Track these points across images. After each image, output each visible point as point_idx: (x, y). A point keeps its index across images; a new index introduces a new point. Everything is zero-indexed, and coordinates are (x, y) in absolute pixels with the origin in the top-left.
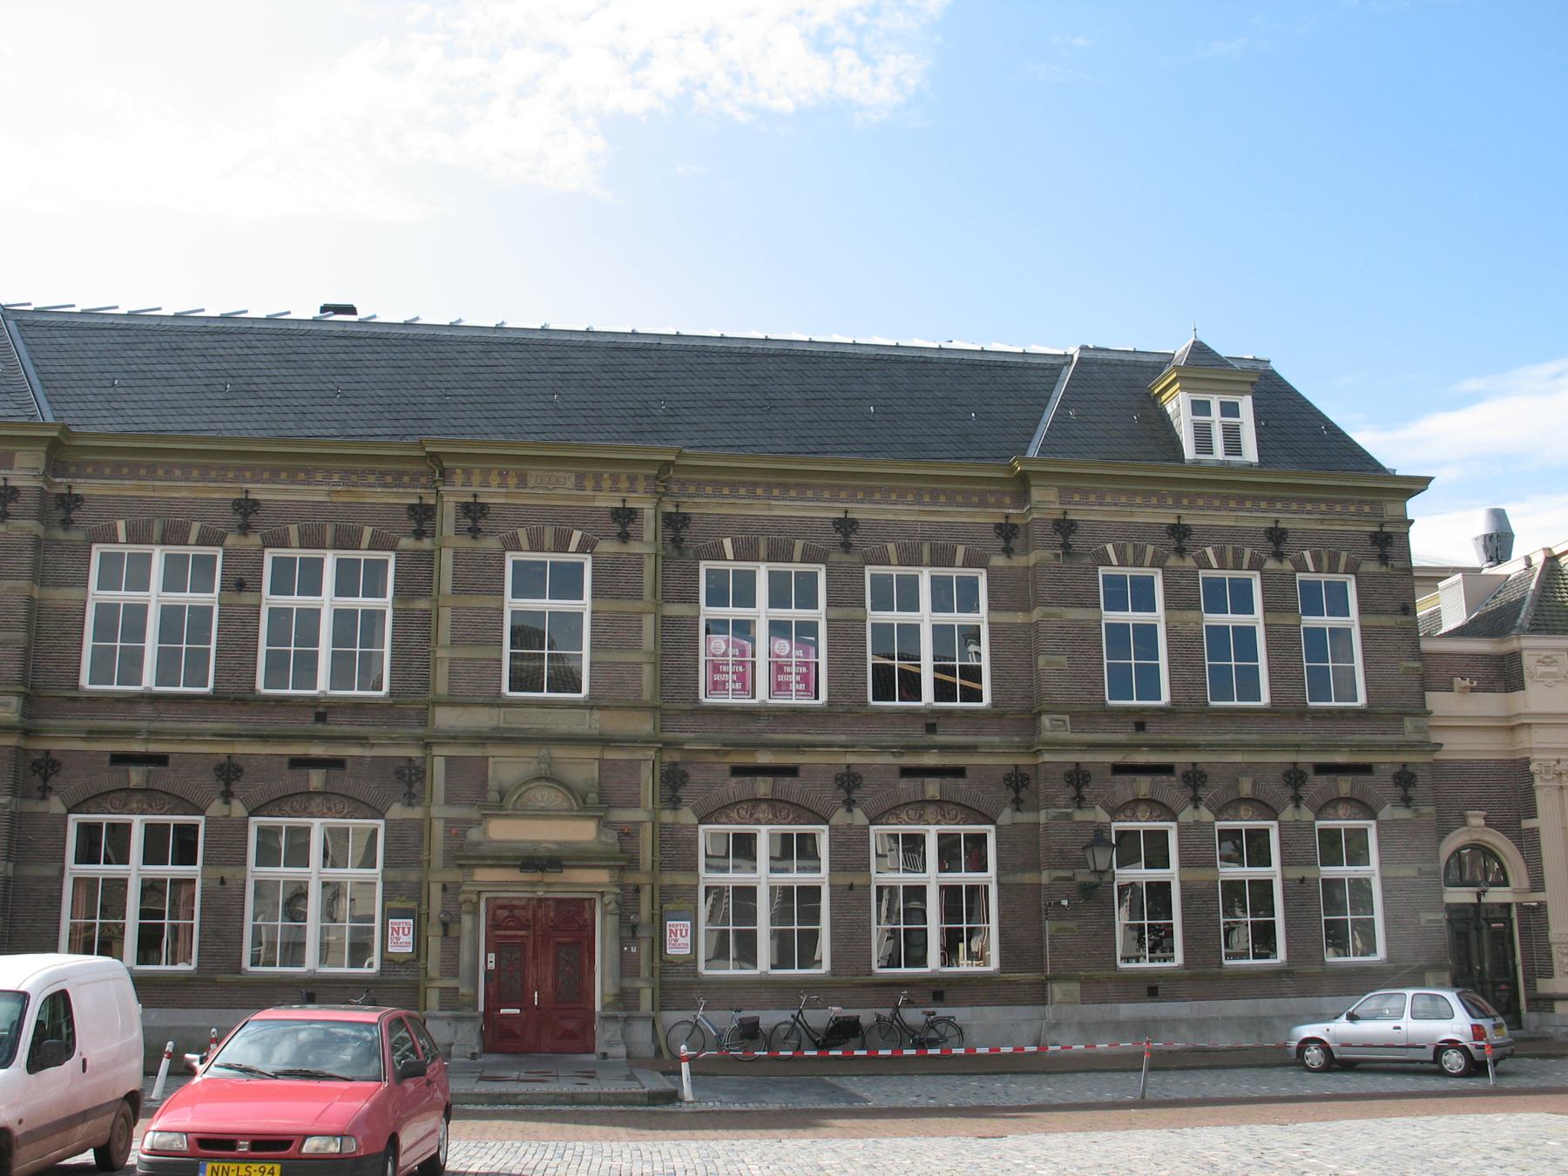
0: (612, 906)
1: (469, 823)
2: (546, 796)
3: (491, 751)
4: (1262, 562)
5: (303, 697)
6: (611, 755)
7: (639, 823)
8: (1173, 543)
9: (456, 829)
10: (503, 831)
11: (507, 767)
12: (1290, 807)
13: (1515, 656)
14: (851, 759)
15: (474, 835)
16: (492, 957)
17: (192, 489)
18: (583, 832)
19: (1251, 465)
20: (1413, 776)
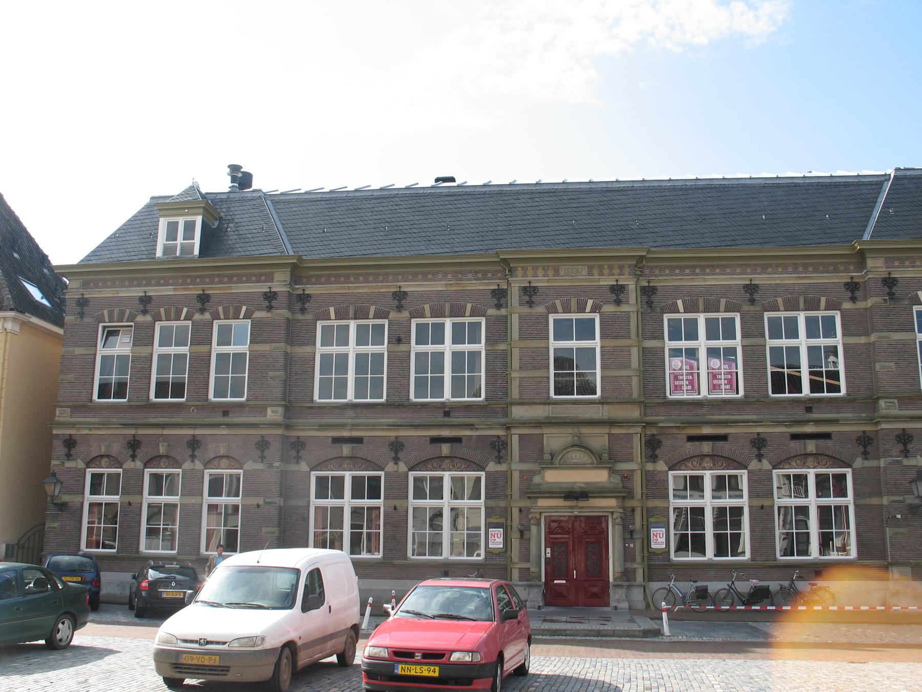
0: (619, 520)
1: (534, 473)
2: (578, 456)
3: (545, 431)
6: (615, 431)
7: (633, 471)
9: (526, 476)
10: (553, 477)
14: (73, 432)
15: (537, 479)
16: (549, 550)
18: (600, 477)
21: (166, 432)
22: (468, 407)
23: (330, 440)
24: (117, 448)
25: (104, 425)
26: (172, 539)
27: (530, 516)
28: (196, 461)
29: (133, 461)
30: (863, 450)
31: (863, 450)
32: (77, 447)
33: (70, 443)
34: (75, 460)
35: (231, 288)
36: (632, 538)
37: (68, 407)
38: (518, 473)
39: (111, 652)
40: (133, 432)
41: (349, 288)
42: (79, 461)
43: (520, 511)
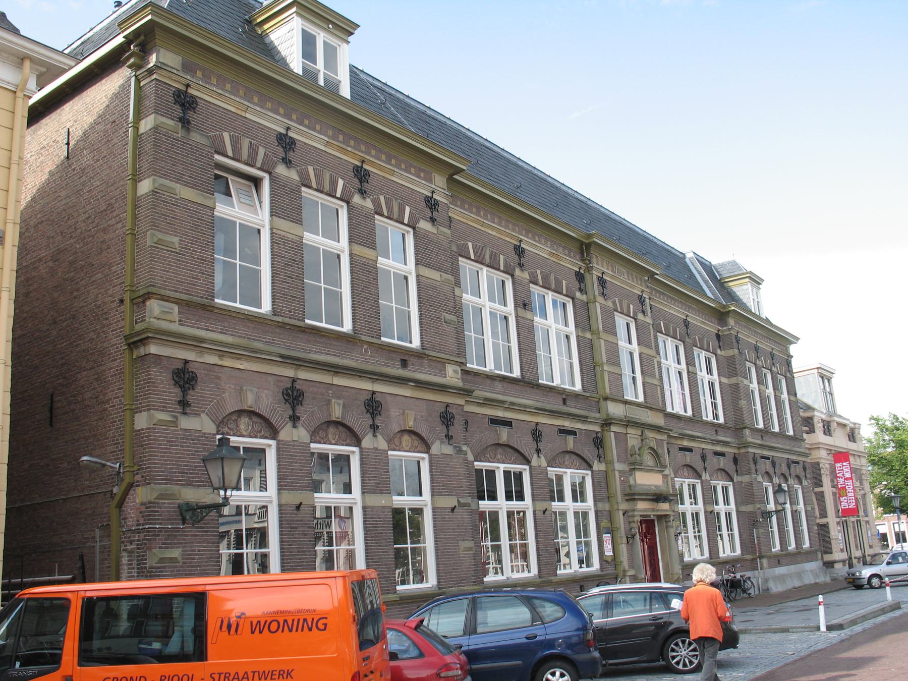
4: (274, 165)
5: (402, 346)
8: (280, 152)
12: (370, 435)
14: (190, 355)
17: (498, 231)
20: (379, 404)
21: (339, 381)
22: (504, 379)
23: (487, 420)
24: (265, 400)
25: (254, 355)
26: (525, 556)
28: (380, 437)
29: (295, 426)
30: (291, 413)
31: (291, 413)
32: (198, 388)
33: (185, 377)
34: (196, 414)
35: (393, 173)
37: (178, 302)
40: (290, 372)
41: (483, 224)
42: (204, 416)
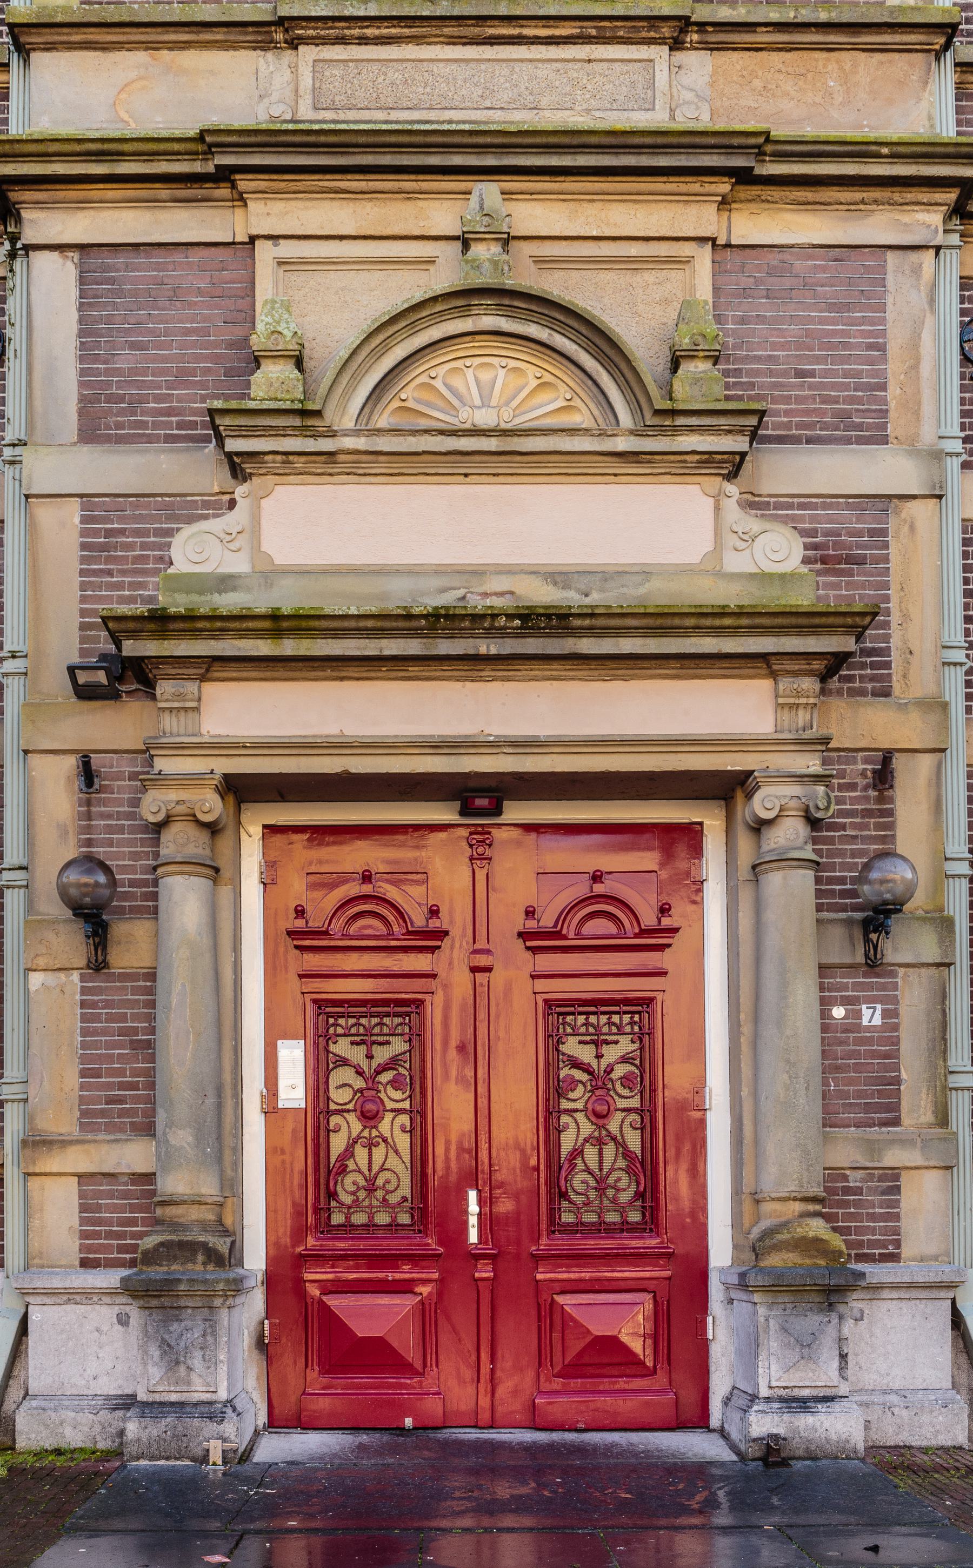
0: (790, 834)
1: (182, 509)
2: (493, 386)
3: (267, 213)
6: (757, 225)
7: (886, 501)
9: (119, 530)
10: (313, 534)
11: (328, 278)
13: (80, 657)
15: (199, 552)
16: (293, 1056)
18: (662, 533)
19: (210, 174)
27: (153, 805)
36: (873, 964)
38: (73, 513)
39: (866, 1549)
43: (88, 773)
